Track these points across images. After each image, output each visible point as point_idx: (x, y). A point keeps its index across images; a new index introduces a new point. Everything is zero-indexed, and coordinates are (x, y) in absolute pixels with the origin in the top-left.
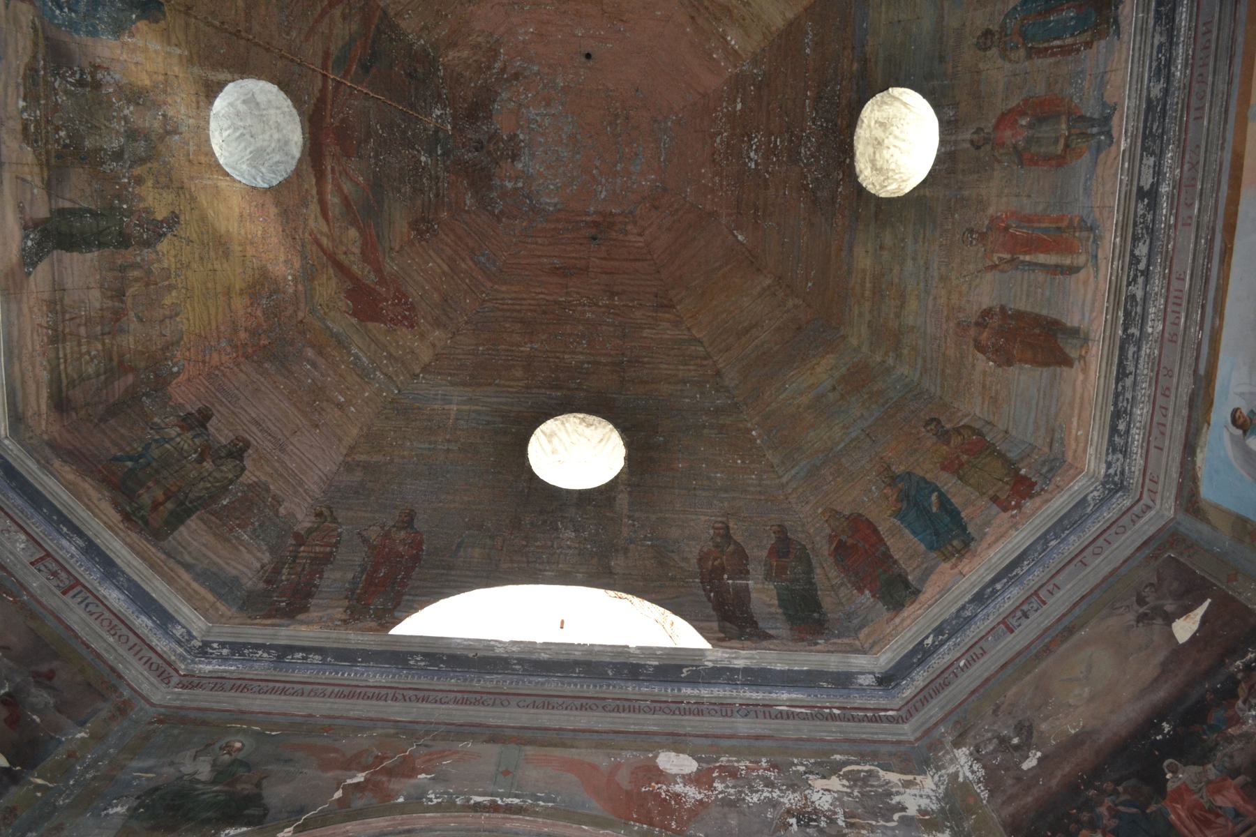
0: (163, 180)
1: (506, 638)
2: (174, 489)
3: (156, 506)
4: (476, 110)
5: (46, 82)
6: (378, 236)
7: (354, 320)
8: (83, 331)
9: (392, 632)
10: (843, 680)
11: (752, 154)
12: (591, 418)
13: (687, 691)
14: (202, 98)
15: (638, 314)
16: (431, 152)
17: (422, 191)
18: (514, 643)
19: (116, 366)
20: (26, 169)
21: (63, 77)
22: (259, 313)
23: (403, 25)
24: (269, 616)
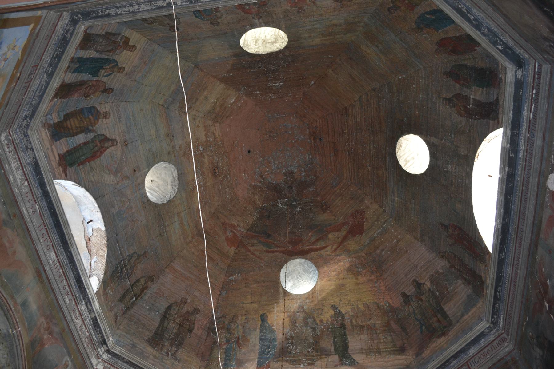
0: (320, 312)
1: (494, 223)
2: (433, 313)
3: (439, 321)
4: (276, 189)
5: (294, 357)
6: (330, 226)
7: (364, 234)
8: (376, 341)
9: (491, 252)
10: (519, 85)
11: (277, 85)
12: (398, 146)
13: (521, 155)
14: (289, 297)
15: (351, 123)
16: (295, 206)
17: (311, 209)
18: (496, 221)
19: (387, 328)
20: (323, 364)
21: (291, 350)
22: (364, 271)
23: (251, 223)
24: (483, 289)
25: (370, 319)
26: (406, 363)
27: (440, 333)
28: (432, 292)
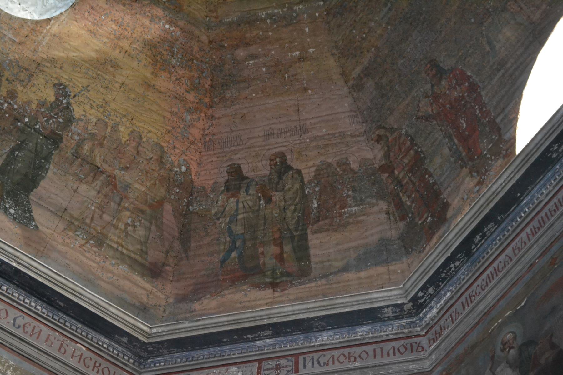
0: (22, 76)
9: (518, 151)
22: (181, 72)
25: (126, 169)
26: (145, 299)
27: (268, 280)
28: (305, 197)
